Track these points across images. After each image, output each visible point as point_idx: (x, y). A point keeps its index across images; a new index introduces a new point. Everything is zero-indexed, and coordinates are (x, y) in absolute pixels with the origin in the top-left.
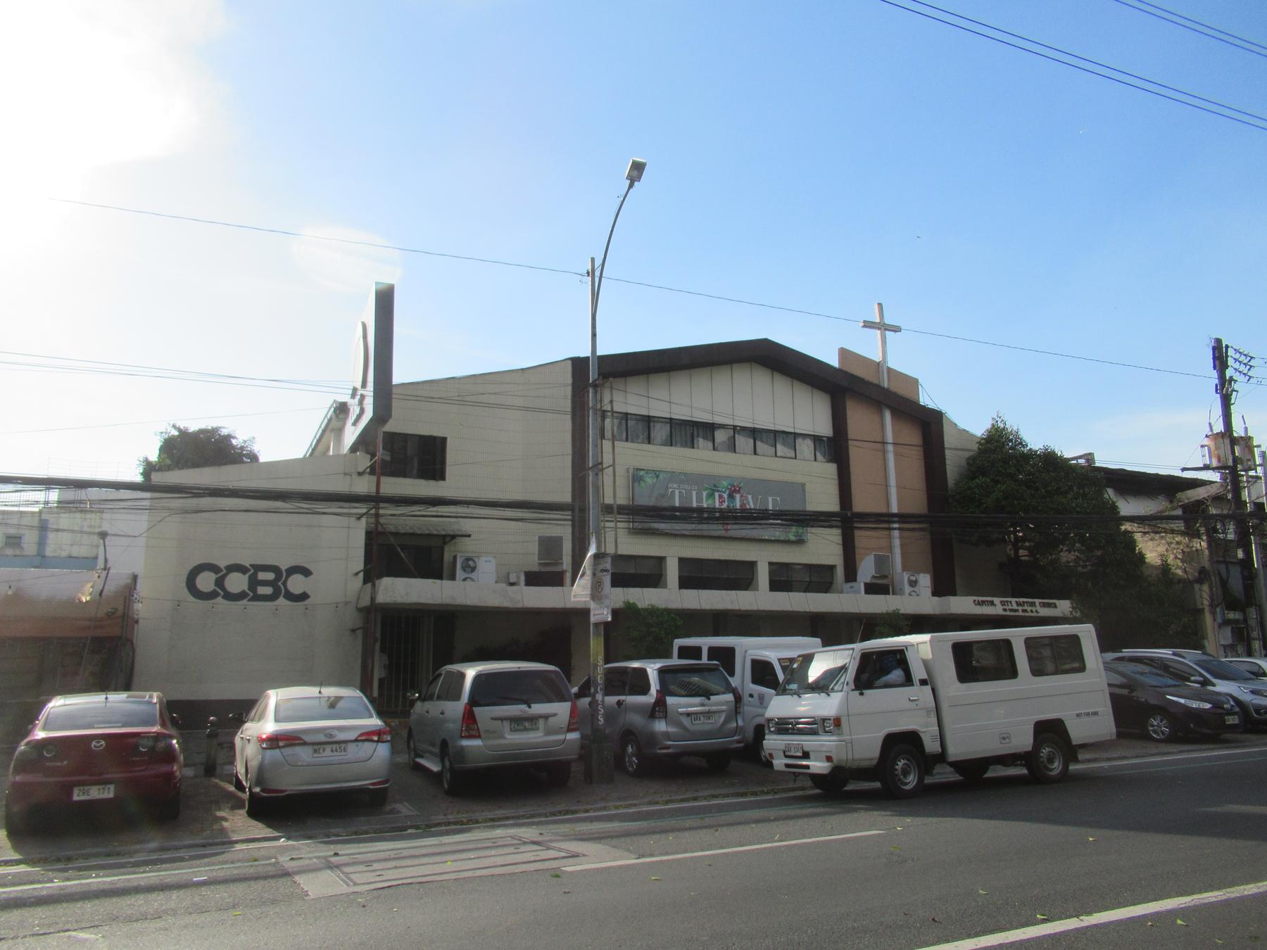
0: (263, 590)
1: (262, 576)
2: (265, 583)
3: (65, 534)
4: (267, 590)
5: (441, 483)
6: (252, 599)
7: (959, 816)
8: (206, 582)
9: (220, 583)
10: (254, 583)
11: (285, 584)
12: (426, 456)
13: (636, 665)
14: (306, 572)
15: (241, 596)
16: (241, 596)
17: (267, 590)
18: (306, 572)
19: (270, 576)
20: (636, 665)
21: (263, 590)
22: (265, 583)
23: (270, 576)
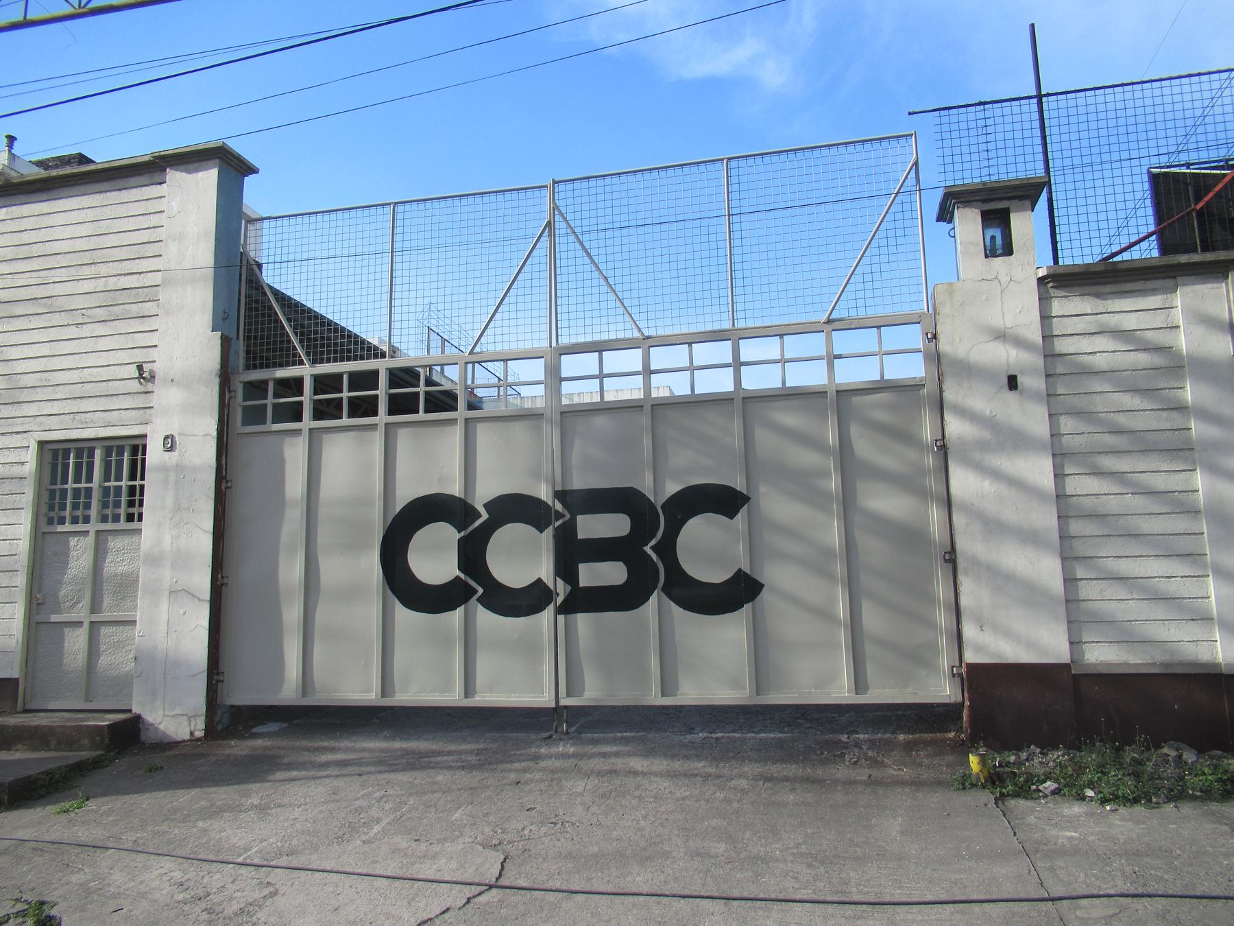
0: (595, 574)
1: (592, 526)
2: (603, 550)
3: (1064, 902)
4: (612, 573)
5: (1159, 163)
6: (567, 608)
7: (939, 705)
8: (434, 558)
9: (472, 555)
10: (570, 553)
11: (668, 549)
12: (177, 508)
13: (654, 557)
14: (726, 501)
15: (530, 600)
16: (530, 600)
17: (612, 573)
18: (726, 501)
19: (614, 525)
20: (654, 557)
21: (595, 574)
22: (603, 550)
23: (614, 525)
